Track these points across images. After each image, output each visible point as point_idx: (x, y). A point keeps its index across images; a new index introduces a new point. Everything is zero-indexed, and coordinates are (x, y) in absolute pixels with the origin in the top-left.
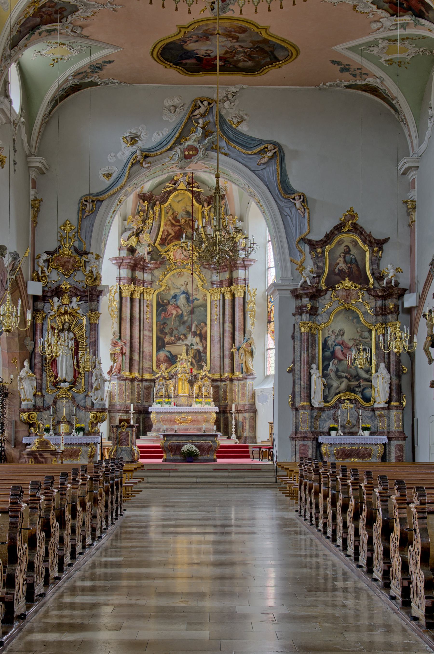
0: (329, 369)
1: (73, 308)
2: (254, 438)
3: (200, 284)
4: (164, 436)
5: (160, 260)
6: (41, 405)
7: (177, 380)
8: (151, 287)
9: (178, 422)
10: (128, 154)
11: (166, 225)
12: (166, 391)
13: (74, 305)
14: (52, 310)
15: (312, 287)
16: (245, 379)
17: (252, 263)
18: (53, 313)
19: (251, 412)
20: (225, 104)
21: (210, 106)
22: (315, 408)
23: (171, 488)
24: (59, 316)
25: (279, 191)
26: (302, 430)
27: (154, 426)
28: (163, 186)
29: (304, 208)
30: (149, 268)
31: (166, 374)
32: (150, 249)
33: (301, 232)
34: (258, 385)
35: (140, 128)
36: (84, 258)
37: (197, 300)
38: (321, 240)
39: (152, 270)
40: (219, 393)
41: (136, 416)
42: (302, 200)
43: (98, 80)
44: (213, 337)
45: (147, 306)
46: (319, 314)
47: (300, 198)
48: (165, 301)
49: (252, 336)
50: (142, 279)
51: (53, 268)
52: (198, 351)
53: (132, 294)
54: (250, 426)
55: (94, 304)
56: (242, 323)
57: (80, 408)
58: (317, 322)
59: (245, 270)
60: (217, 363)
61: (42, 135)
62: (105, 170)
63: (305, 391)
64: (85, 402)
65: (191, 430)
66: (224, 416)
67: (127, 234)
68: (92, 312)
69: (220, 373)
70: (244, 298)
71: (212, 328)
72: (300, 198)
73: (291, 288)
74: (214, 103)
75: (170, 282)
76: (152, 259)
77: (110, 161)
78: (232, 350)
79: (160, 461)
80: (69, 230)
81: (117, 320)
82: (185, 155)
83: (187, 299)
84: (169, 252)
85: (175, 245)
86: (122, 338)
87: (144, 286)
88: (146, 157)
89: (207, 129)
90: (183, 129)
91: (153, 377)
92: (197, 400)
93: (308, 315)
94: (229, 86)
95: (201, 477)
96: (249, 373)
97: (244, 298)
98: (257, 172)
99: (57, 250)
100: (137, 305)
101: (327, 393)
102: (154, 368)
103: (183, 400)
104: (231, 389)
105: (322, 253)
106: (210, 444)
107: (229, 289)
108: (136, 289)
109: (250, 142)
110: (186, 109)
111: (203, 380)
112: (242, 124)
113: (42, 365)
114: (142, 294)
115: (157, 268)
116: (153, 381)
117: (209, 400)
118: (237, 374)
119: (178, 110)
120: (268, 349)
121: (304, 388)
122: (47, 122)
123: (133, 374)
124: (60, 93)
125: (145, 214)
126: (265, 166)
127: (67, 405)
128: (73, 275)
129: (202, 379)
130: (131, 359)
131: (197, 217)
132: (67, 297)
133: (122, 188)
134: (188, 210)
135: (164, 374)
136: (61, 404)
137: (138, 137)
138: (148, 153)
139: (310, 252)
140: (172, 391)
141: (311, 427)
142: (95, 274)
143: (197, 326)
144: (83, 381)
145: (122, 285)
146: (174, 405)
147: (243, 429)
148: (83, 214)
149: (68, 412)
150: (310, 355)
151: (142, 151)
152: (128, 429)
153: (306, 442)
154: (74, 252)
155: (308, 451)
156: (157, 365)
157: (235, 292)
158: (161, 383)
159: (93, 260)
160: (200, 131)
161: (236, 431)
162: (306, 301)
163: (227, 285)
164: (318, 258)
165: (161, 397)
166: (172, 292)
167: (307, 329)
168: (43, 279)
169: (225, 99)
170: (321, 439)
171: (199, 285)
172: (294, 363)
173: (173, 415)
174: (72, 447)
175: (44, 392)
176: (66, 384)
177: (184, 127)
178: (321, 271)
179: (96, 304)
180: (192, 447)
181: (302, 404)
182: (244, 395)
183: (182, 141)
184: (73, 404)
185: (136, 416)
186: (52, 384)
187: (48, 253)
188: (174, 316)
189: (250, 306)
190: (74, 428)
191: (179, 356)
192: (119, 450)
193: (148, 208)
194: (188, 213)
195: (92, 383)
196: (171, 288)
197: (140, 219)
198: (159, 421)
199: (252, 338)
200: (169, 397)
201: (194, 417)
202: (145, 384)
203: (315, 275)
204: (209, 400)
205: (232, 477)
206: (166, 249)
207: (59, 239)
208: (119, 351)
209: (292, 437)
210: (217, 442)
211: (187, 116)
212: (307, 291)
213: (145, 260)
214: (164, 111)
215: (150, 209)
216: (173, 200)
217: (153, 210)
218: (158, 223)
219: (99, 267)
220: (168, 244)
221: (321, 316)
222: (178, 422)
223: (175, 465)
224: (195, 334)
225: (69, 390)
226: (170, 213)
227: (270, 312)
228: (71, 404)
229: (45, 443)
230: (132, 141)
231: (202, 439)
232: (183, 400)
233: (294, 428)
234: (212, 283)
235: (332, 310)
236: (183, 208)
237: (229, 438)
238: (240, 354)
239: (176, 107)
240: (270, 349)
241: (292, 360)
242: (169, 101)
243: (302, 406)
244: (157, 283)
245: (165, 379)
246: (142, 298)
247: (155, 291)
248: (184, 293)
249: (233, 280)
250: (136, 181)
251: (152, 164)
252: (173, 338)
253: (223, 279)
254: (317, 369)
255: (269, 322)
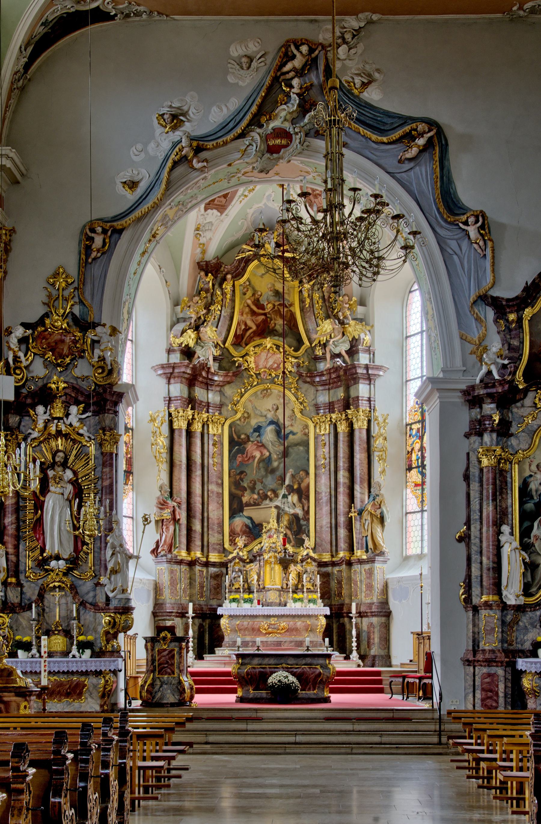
0: (532, 535)
1: (71, 425)
2: (387, 660)
3: (297, 407)
4: (238, 656)
5: (234, 369)
6: (16, 600)
7: (262, 563)
8: (220, 414)
9: (264, 632)
10: (166, 145)
11: (242, 314)
12: (246, 580)
13: (73, 419)
14: (33, 430)
15: (502, 382)
16: (371, 561)
17: (381, 373)
18: (35, 434)
19: (381, 616)
20: (340, 49)
21: (313, 55)
22: (510, 606)
23: (250, 754)
24: (47, 440)
25: (438, 209)
26: (487, 648)
27: (226, 639)
28: (237, 249)
29: (485, 241)
30: (216, 383)
31: (245, 553)
32: (217, 352)
33: (478, 284)
34: (393, 571)
35: (188, 99)
36: (91, 335)
37: (294, 434)
38: (517, 298)
39: (222, 385)
40: (329, 584)
41: (197, 621)
42: (479, 224)
43: (110, 7)
44: (319, 493)
45: (214, 445)
46: (512, 435)
47: (477, 221)
48: (243, 436)
49: (381, 492)
50: (206, 400)
51: (35, 354)
52: (296, 516)
53: (189, 424)
54: (380, 638)
55: (108, 417)
56: (366, 470)
57: (85, 607)
58: (510, 450)
59: (370, 384)
60: (326, 536)
61: (14, 112)
62: (126, 175)
63: (491, 573)
64: (95, 596)
65: (286, 644)
66: (339, 621)
67: (180, 327)
68: (104, 430)
69: (331, 552)
70: (368, 431)
71: (318, 479)
72: (477, 221)
73: (464, 387)
74: (320, 48)
75: (250, 406)
76: (220, 368)
77: (135, 158)
78: (351, 514)
79: (231, 698)
80: (63, 285)
81: (165, 467)
82: (268, 145)
83: (278, 433)
84: (248, 358)
85: (258, 345)
86: (175, 495)
87: (208, 412)
88: (198, 150)
89: (307, 98)
90: (264, 99)
91: (224, 559)
92: (295, 596)
93: (494, 435)
94: (347, 18)
95: (305, 732)
96: (378, 552)
97: (368, 431)
98: (398, 176)
99: (41, 322)
100: (197, 442)
101: (530, 579)
102: (227, 545)
103: (272, 596)
104: (350, 579)
105: (517, 322)
106: (317, 671)
107: (344, 415)
108: (196, 416)
109: (386, 120)
110: (268, 62)
111: (304, 563)
112: (370, 88)
113: (18, 529)
114: (205, 425)
115: (229, 383)
116: (224, 565)
117: (315, 596)
118: (359, 553)
119: (254, 64)
120: (407, 513)
121: (489, 569)
122: (23, 89)
123: (192, 553)
124: (40, 30)
125: (209, 295)
126: (412, 164)
127: (63, 601)
128: (71, 366)
129: (302, 561)
130: (189, 530)
131: (291, 300)
132: (60, 405)
133: (156, 207)
134: (277, 288)
135: (241, 554)
136: (52, 599)
137: (185, 114)
138: (201, 143)
139: (496, 321)
140: (255, 582)
141: (503, 641)
142: (109, 364)
143: (293, 476)
144: (91, 557)
145: (172, 409)
146: (259, 604)
147: (369, 643)
148: (88, 255)
149: (64, 613)
150: (498, 508)
151: (192, 139)
152: (173, 644)
153: (493, 670)
154: (71, 323)
155: (497, 686)
156: (230, 540)
157: (354, 420)
158: (237, 568)
159: (105, 339)
160: (295, 99)
161: (358, 647)
162: (489, 408)
163: (341, 408)
164: (510, 330)
165: (237, 591)
166: (254, 422)
167: (493, 461)
168: (18, 372)
169: (340, 41)
170: (522, 664)
171: (297, 411)
172: (468, 523)
173: (258, 620)
174: (71, 677)
175: (22, 577)
176: (61, 562)
177: (267, 94)
178: (516, 355)
179: (113, 419)
180: (286, 677)
181: (484, 598)
182: (370, 587)
183: (263, 119)
184: (74, 598)
185: (197, 621)
186: (36, 563)
187: (26, 326)
188: (256, 460)
189: (377, 443)
190: (75, 643)
191: (265, 525)
192: (158, 683)
193: (213, 285)
194: (277, 293)
195: (106, 560)
196: (252, 415)
197: (201, 303)
198: (234, 630)
199: (383, 496)
200: (250, 591)
201: (291, 623)
202: (212, 570)
203: (506, 362)
204: (315, 596)
205: (359, 732)
206: (243, 352)
207: (46, 301)
208: (170, 517)
209: (468, 661)
210: (330, 666)
211: (272, 73)
212: (494, 390)
213: (209, 368)
214: (229, 65)
215: (216, 287)
216: (253, 273)
217: (222, 289)
218: (229, 311)
219: (114, 350)
220: (246, 345)
221: (517, 437)
222: (264, 632)
223: (256, 710)
224: (291, 490)
225: (65, 574)
226: (249, 293)
227: (410, 453)
228: (70, 599)
229: (5, 674)
230: (173, 121)
231: (304, 662)
232: (272, 596)
233: (471, 643)
234: (317, 408)
235: (536, 427)
236: (269, 286)
237: (347, 658)
238: (363, 521)
239: (251, 59)
240: (410, 513)
241: (464, 520)
242: (238, 48)
243: (486, 602)
244: (229, 407)
245: (243, 560)
246: (206, 431)
247: (226, 420)
248: (272, 423)
249: (351, 401)
250: (181, 197)
251: (210, 164)
252: (256, 496)
253: (335, 399)
254: (512, 534)
255: (410, 469)
